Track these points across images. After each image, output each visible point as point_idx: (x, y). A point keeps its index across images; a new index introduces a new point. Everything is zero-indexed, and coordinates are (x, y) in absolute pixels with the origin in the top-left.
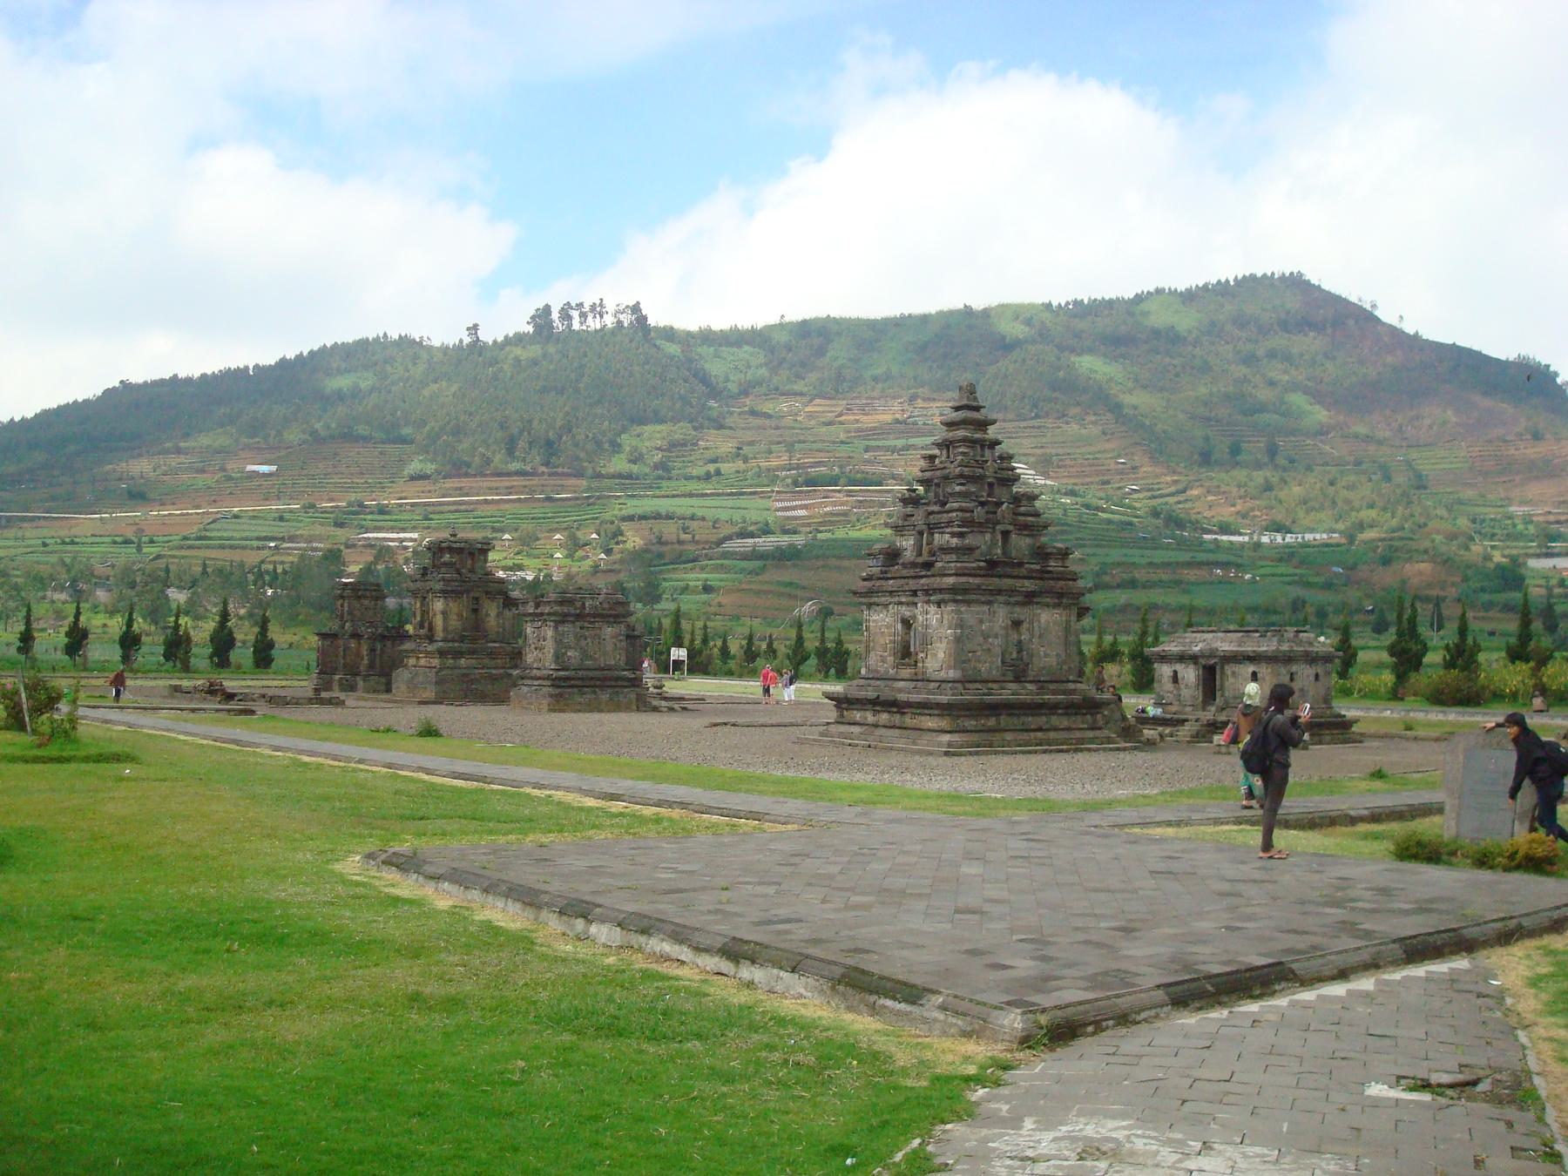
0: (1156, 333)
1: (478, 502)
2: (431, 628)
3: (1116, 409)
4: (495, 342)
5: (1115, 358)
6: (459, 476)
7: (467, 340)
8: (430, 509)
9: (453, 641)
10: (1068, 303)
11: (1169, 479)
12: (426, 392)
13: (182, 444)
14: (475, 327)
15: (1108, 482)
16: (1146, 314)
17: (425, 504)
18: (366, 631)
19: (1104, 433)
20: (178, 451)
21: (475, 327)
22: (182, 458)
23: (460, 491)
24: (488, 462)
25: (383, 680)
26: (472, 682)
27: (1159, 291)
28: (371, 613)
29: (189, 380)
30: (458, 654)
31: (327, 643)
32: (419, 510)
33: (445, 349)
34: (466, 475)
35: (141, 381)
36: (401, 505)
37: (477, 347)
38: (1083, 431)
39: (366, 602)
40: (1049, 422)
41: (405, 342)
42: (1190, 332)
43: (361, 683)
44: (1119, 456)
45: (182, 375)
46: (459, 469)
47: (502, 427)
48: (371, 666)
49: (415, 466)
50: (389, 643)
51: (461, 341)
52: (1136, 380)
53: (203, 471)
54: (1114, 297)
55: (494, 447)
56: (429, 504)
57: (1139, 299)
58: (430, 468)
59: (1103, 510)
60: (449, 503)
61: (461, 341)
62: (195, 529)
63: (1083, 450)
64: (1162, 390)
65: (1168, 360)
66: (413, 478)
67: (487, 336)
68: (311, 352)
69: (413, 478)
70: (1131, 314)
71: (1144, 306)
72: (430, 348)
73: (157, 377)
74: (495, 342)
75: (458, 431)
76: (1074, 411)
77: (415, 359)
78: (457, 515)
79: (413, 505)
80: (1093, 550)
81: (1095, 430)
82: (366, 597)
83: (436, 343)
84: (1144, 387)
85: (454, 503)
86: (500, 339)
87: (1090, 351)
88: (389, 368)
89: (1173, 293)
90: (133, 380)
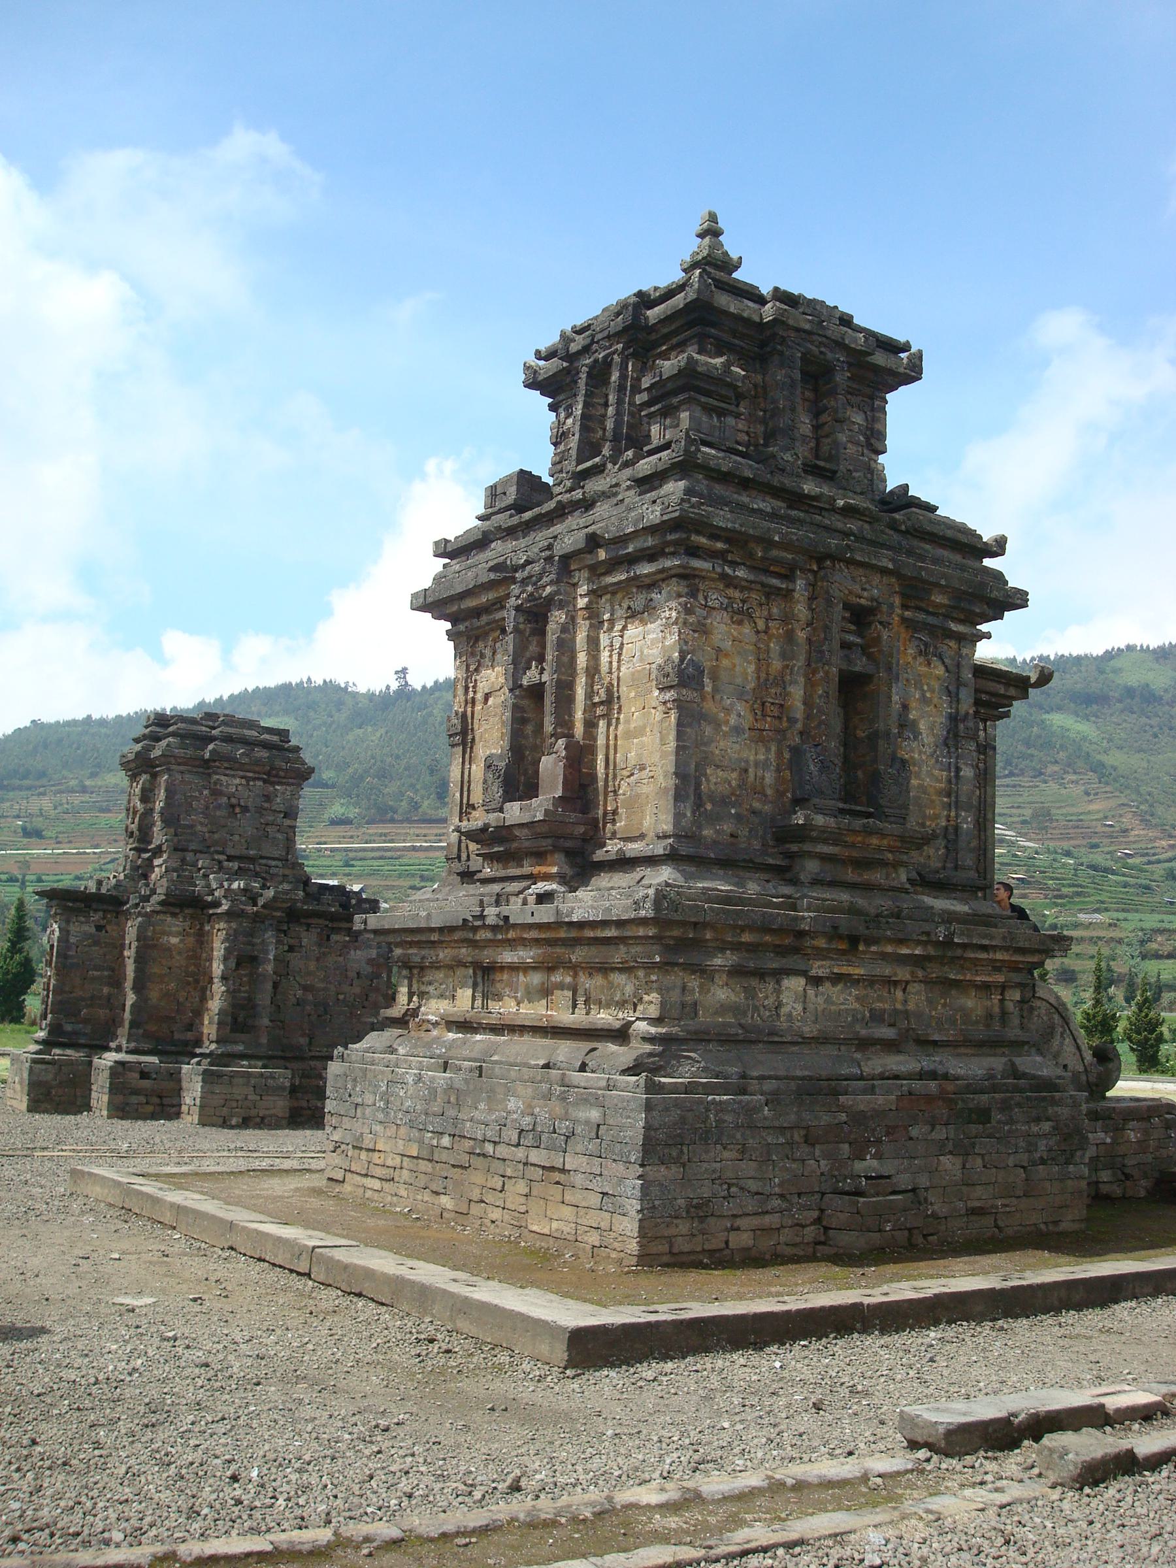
0: (1130, 692)
1: (405, 849)
2: (582, 789)
3: (1098, 769)
4: (424, 687)
5: (1086, 718)
6: (383, 821)
7: (394, 686)
8: (351, 855)
9: (727, 863)
10: (1033, 659)
11: (1164, 843)
12: (350, 737)
13: (87, 783)
14: (404, 671)
15: (1096, 846)
16: (1116, 671)
17: (346, 850)
18: (222, 888)
19: (1088, 794)
20: (84, 790)
21: (404, 671)
22: (86, 797)
23: (384, 837)
24: (416, 806)
25: (282, 1076)
26: (862, 1133)
27: (1130, 648)
28: (246, 826)
29: (102, 722)
30: (776, 949)
31: (82, 928)
32: (339, 856)
33: (370, 696)
34: (392, 821)
35: (52, 721)
36: (319, 850)
37: (405, 693)
38: (1064, 791)
39: (232, 783)
40: (1025, 781)
41: (329, 688)
42: (1166, 691)
43: (193, 1090)
44: (1106, 818)
45: (96, 716)
46: (383, 814)
47: (432, 771)
48: (238, 1020)
49: (337, 809)
50: (308, 939)
51: (388, 687)
52: (1110, 740)
53: (108, 810)
54: (1082, 652)
55: (423, 792)
56: (351, 850)
57: (1109, 655)
58: (353, 812)
59: (1113, 873)
60: (373, 849)
61: (388, 687)
62: (90, 868)
63: (1064, 811)
64: (1140, 750)
65: (1144, 720)
66: (334, 822)
67: (416, 681)
68: (231, 696)
69: (334, 822)
70: (1102, 672)
71: (1115, 663)
72: (355, 695)
73: (69, 718)
74: (424, 687)
75: (383, 775)
76: (1051, 769)
77: (340, 704)
78: (382, 862)
79: (332, 850)
80: (1121, 915)
81: (1079, 790)
82: (233, 765)
83: (362, 689)
84: (1120, 748)
85: (379, 849)
86: (429, 684)
87: (1059, 709)
88: (312, 714)
89: (1146, 650)
90: (45, 720)
